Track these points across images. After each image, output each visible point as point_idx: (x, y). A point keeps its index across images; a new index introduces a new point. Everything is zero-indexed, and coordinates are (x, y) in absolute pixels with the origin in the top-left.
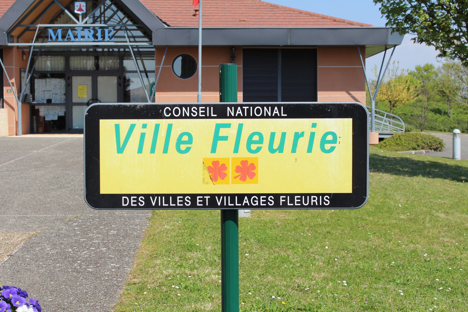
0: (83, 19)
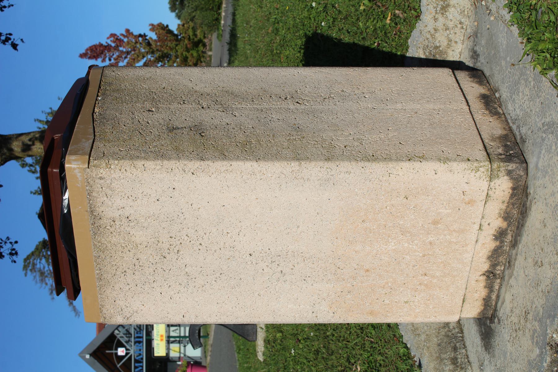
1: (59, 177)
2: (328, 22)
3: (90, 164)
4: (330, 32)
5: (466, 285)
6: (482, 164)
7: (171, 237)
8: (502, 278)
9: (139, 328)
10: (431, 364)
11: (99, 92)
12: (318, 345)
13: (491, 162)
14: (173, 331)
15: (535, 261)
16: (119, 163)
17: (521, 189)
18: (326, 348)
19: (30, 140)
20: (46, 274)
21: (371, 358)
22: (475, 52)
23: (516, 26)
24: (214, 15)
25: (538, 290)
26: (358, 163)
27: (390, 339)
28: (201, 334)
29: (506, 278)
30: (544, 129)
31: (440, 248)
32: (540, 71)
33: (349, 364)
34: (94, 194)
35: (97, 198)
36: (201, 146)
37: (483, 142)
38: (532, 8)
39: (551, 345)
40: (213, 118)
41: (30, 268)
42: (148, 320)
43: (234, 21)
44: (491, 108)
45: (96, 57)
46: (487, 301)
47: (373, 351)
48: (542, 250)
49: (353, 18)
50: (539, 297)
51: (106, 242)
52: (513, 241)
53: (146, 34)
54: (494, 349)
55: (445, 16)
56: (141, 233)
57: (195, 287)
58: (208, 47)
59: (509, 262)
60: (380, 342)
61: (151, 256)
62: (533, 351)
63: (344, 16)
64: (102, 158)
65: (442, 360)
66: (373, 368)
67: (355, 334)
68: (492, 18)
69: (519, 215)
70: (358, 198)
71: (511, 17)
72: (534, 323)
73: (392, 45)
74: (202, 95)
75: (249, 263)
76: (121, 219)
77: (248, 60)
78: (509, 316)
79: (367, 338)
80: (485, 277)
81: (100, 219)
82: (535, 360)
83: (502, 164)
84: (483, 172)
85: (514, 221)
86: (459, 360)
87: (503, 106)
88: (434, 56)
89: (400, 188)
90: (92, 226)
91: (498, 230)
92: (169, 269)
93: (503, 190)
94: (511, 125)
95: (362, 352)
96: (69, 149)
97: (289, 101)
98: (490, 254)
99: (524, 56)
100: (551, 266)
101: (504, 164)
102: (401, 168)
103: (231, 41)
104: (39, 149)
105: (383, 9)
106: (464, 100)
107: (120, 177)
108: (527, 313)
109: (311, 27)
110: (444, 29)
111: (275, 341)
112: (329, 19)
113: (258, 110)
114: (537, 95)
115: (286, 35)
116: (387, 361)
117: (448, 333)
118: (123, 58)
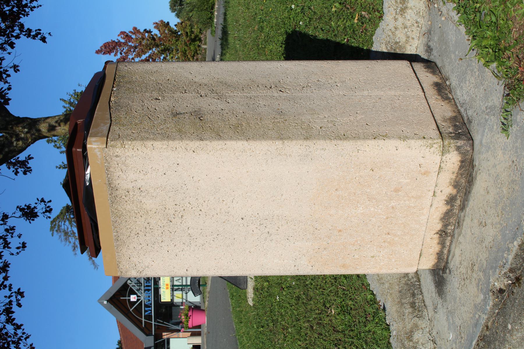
0: (140, 297)
1: (82, 156)
2: (305, 21)
3: (108, 145)
4: (306, 30)
5: (422, 242)
6: (435, 141)
7: (176, 205)
8: (453, 236)
9: (148, 279)
10: (393, 307)
11: (114, 84)
12: (299, 292)
13: (442, 139)
14: (176, 281)
15: (480, 222)
16: (132, 143)
17: (468, 162)
18: (306, 294)
19: (56, 122)
20: (70, 233)
21: (343, 303)
22: (429, 47)
23: (463, 25)
24: (208, 14)
25: (482, 245)
26: (331, 141)
27: (359, 287)
28: (201, 284)
29: (456, 236)
30: (487, 111)
31: (400, 212)
32: (484, 63)
33: (325, 308)
34: (111, 169)
35: (114, 173)
36: (200, 128)
37: (436, 122)
38: (476, 10)
39: (493, 291)
40: (210, 105)
41: (56, 229)
42: (158, 273)
43: (225, 20)
44: (443, 94)
45: (109, 52)
46: (440, 255)
47: (345, 297)
48: (486, 212)
49: (326, 18)
50: (483, 251)
51: (121, 209)
52: (462, 205)
53: (151, 31)
54: (446, 295)
55: (403, 16)
56: (151, 201)
57: (196, 246)
58: (203, 42)
59: (458, 223)
60: (350, 290)
61: (160, 221)
62: (478, 297)
63: (318, 16)
64: (117, 139)
65: (402, 304)
66: (345, 311)
67: (330, 283)
68: (443, 19)
69: (467, 183)
70: (332, 170)
71: (459, 18)
72: (479, 273)
73: (359, 41)
74: (200, 85)
75: (241, 225)
76: (134, 190)
77: (238, 53)
78: (458, 268)
79: (340, 286)
80: (438, 236)
81: (117, 190)
82: (480, 304)
83: (452, 141)
84: (437, 148)
85: (462, 188)
86: (417, 304)
87: (453, 92)
88: (394, 50)
89: (367, 162)
90: (110, 196)
91: (449, 196)
92: (175, 231)
93: (453, 163)
94: (460, 108)
95: (336, 298)
96: (90, 132)
97: (274, 90)
98: (442, 216)
99: (470, 51)
100: (493, 226)
101: (454, 141)
102: (368, 146)
103: (223, 36)
104: (64, 129)
105: (352, 11)
106: (420, 87)
107: (133, 155)
108: (473, 265)
109: (291, 26)
110: (403, 28)
111: (263, 289)
112: (306, 19)
113: (247, 97)
114: (481, 83)
115: (269, 32)
116: (356, 305)
117: (407, 282)
118: (131, 52)
